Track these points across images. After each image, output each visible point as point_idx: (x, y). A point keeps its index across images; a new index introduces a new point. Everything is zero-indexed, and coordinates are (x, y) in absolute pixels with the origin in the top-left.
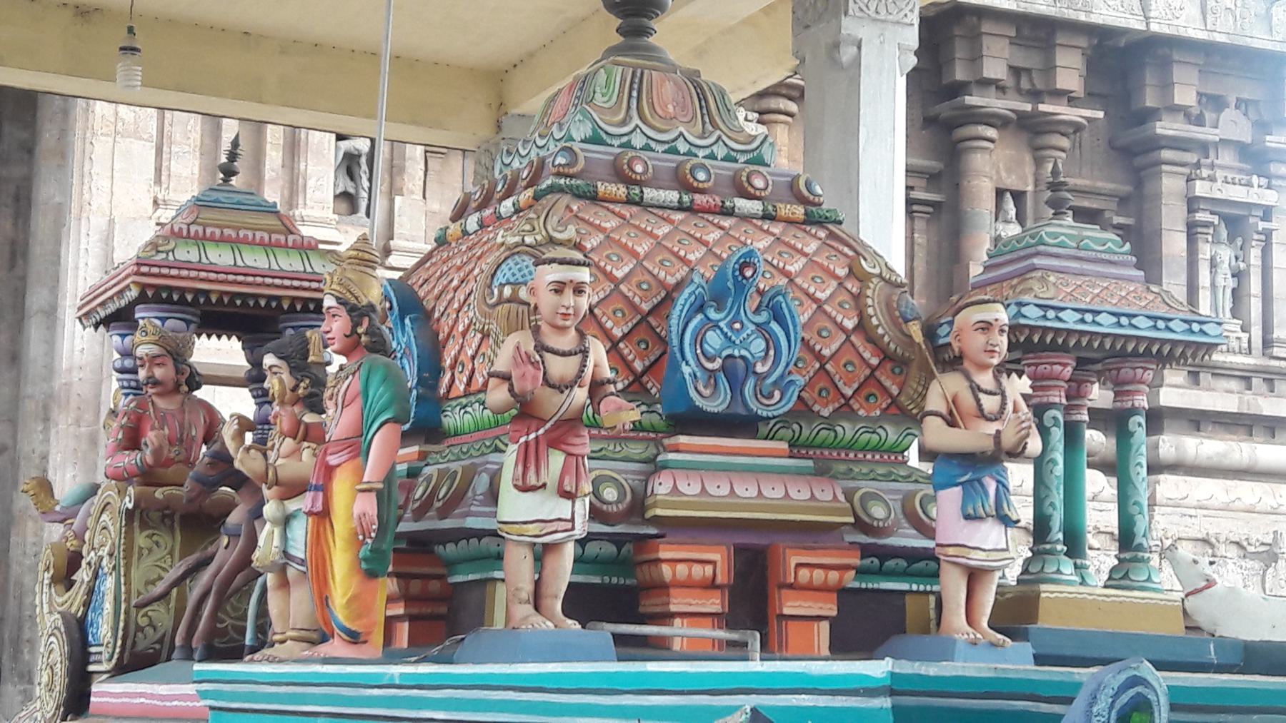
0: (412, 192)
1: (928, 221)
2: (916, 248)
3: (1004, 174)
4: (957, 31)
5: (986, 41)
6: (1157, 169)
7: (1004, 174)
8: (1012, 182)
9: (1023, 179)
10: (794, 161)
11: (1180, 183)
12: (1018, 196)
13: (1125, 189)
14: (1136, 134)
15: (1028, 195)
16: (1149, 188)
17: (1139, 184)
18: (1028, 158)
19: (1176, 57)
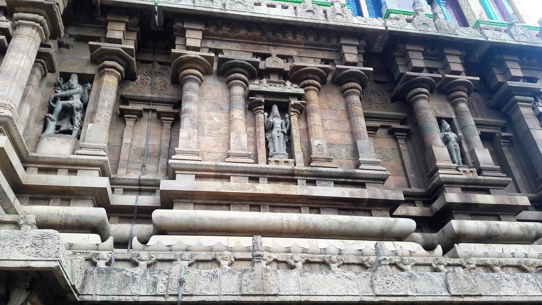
0: (99, 121)
1: (406, 140)
2: (402, 151)
3: (438, 111)
4: (395, 54)
5: (410, 53)
6: (515, 105)
7: (438, 111)
8: (443, 114)
9: (448, 113)
10: (323, 108)
11: (530, 110)
12: (450, 121)
13: (502, 122)
14: (496, 97)
15: (454, 119)
16: (514, 118)
17: (506, 116)
18: (448, 105)
19: (505, 57)
